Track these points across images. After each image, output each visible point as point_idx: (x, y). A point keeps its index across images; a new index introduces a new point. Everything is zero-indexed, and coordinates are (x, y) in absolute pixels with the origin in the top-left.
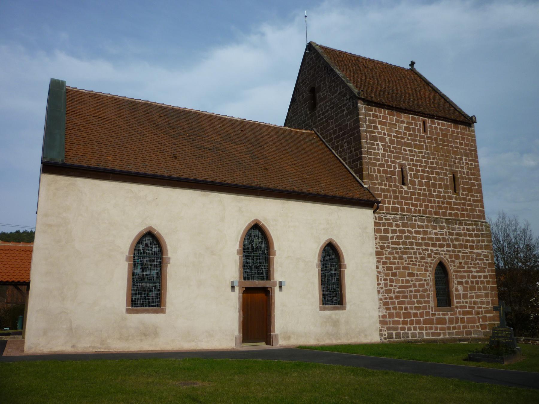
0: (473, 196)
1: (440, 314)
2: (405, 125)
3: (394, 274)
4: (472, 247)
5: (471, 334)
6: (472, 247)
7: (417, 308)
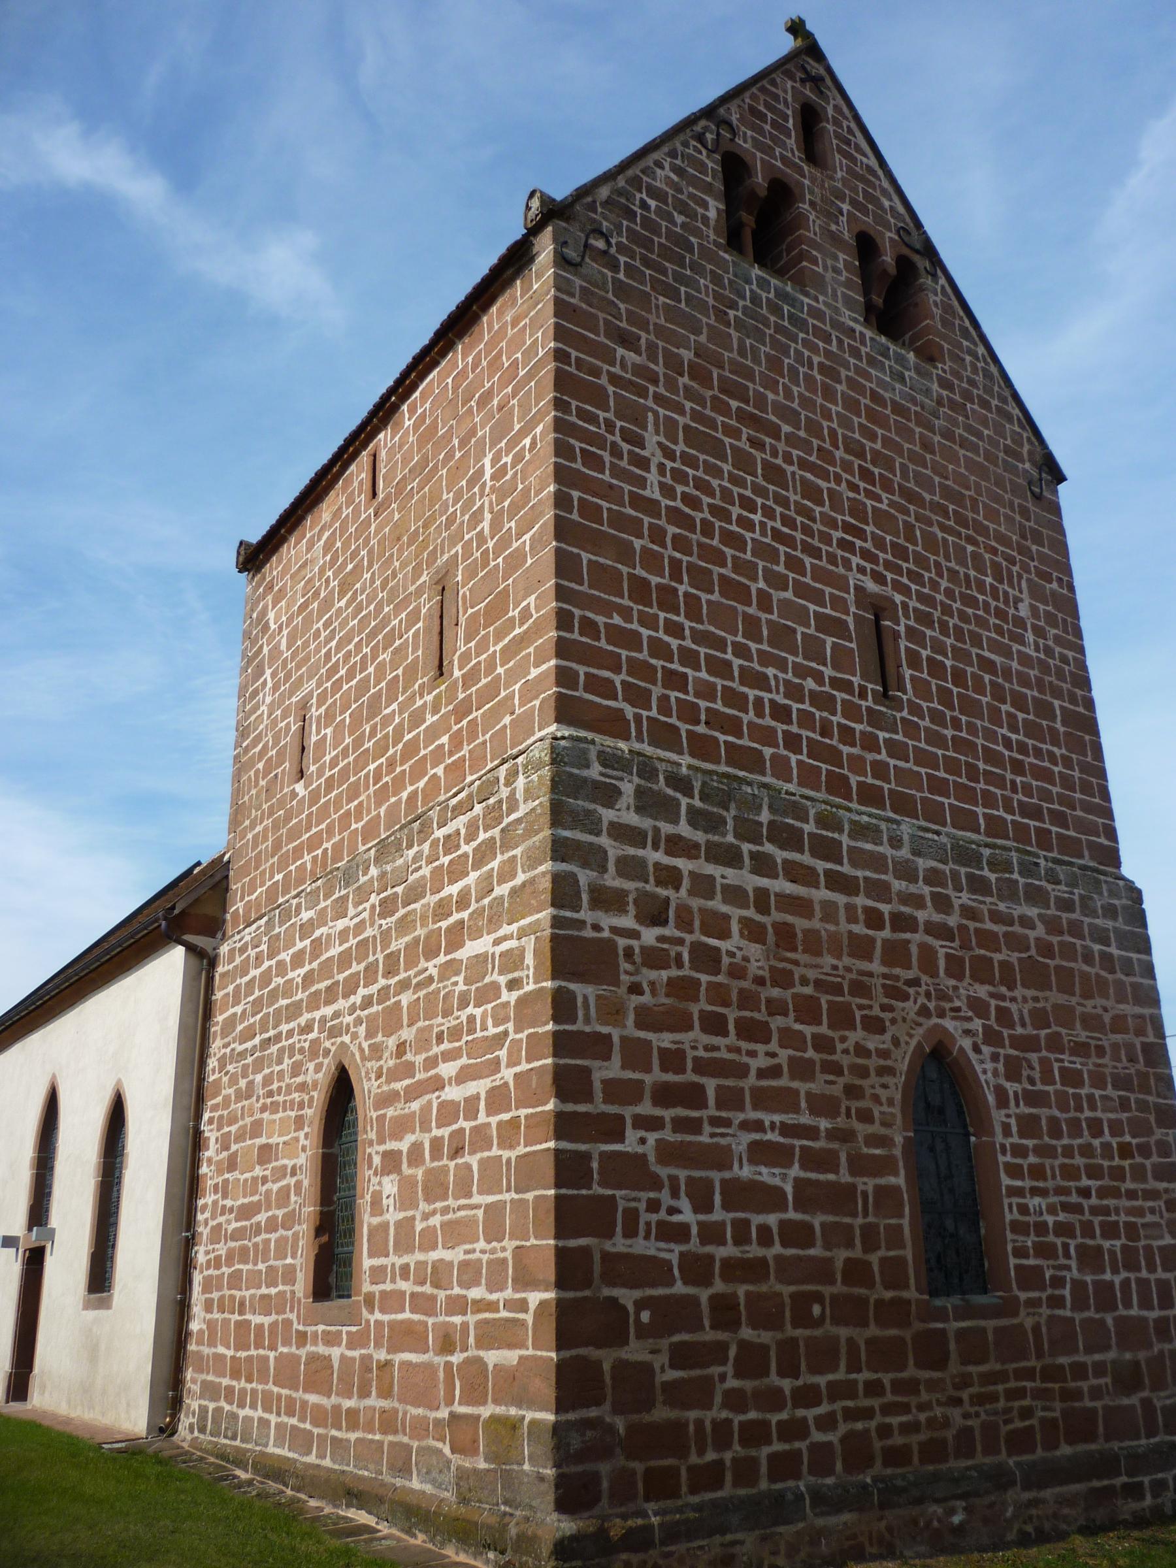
5: (404, 1470)
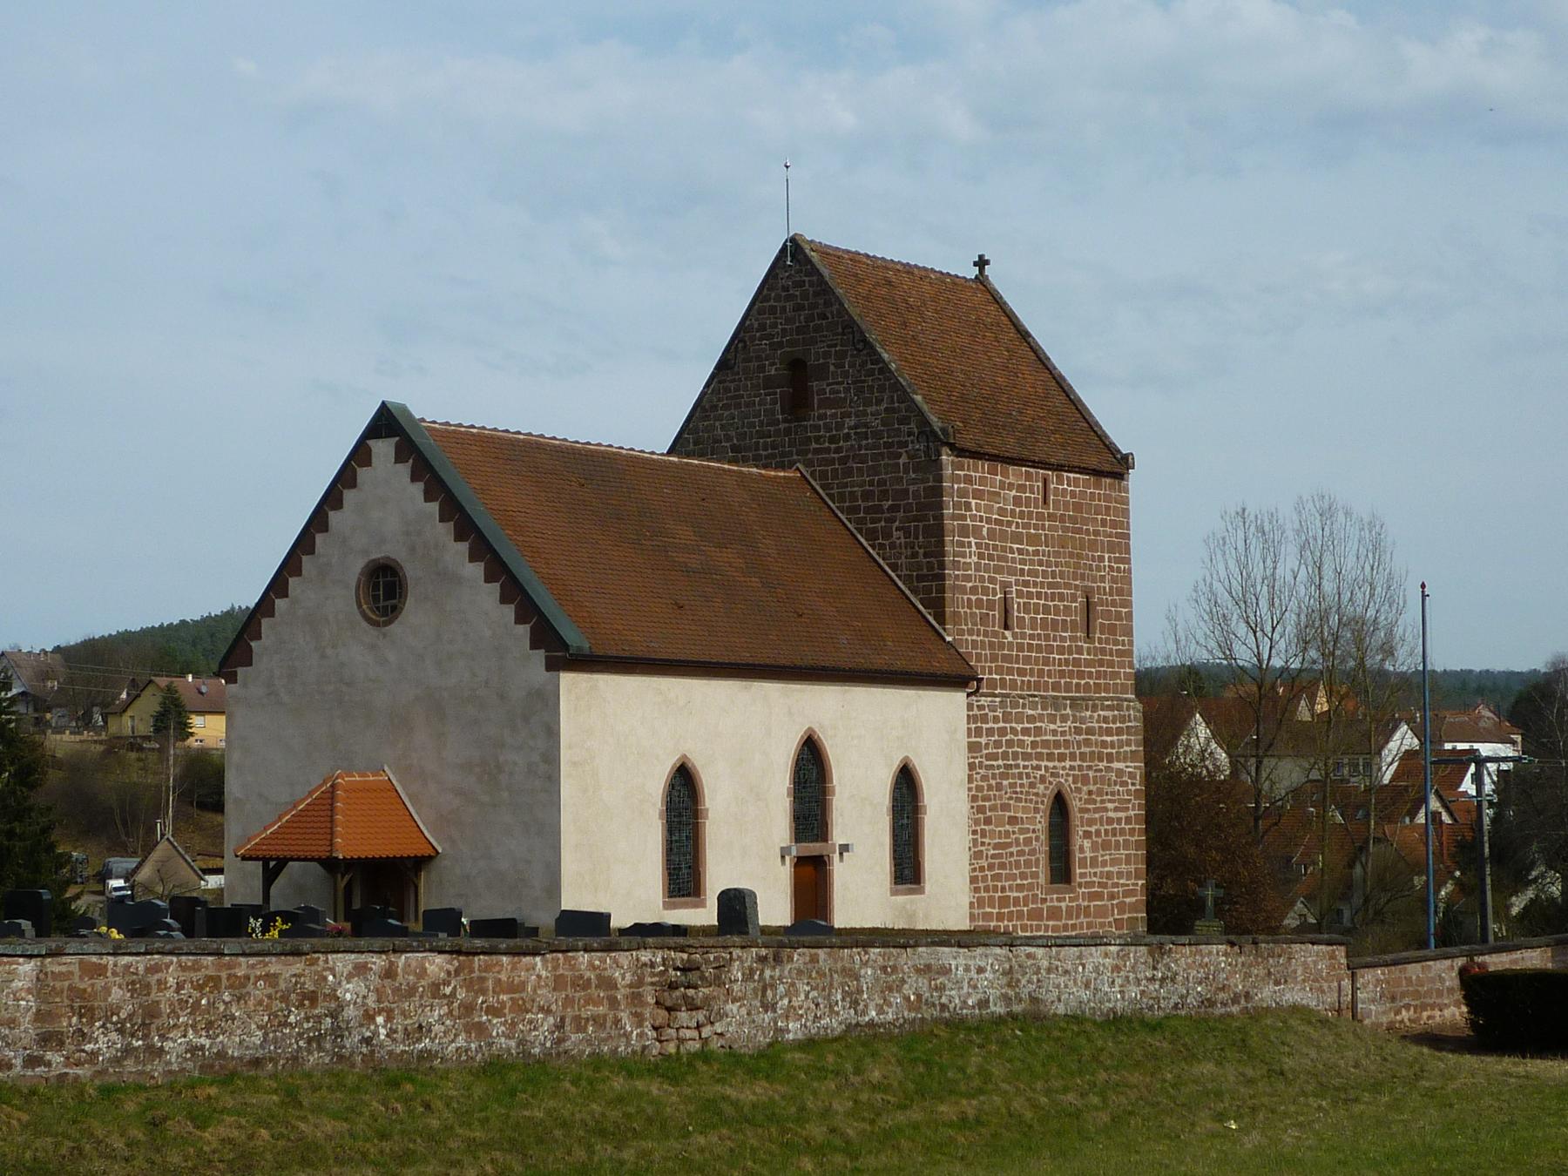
0: (1116, 643)
1: (1053, 900)
2: (1014, 493)
3: (988, 821)
4: (1110, 758)
6: (1110, 758)
7: (1020, 888)
